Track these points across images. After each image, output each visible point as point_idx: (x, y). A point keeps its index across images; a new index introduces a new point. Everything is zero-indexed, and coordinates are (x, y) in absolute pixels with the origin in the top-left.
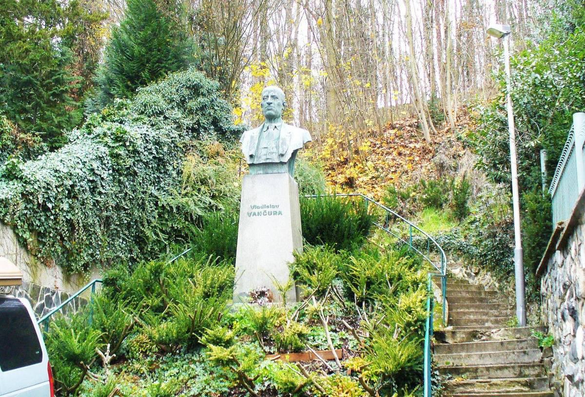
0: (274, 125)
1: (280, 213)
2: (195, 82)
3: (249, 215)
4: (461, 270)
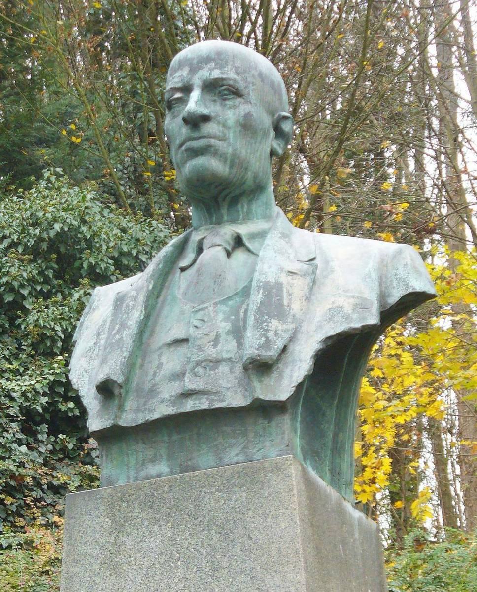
0: (228, 231)
2: (57, 227)
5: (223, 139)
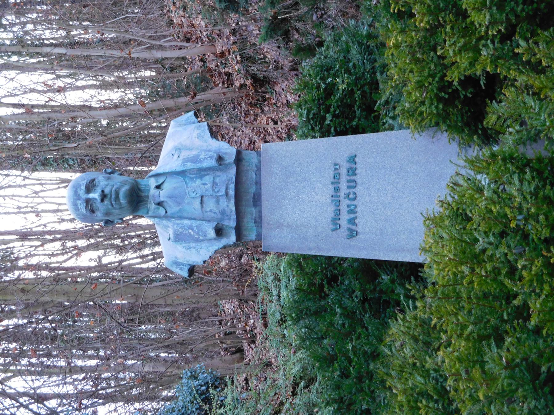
0: (153, 191)
1: (352, 159)
3: (352, 234)
4: (149, 366)
5: (113, 186)
